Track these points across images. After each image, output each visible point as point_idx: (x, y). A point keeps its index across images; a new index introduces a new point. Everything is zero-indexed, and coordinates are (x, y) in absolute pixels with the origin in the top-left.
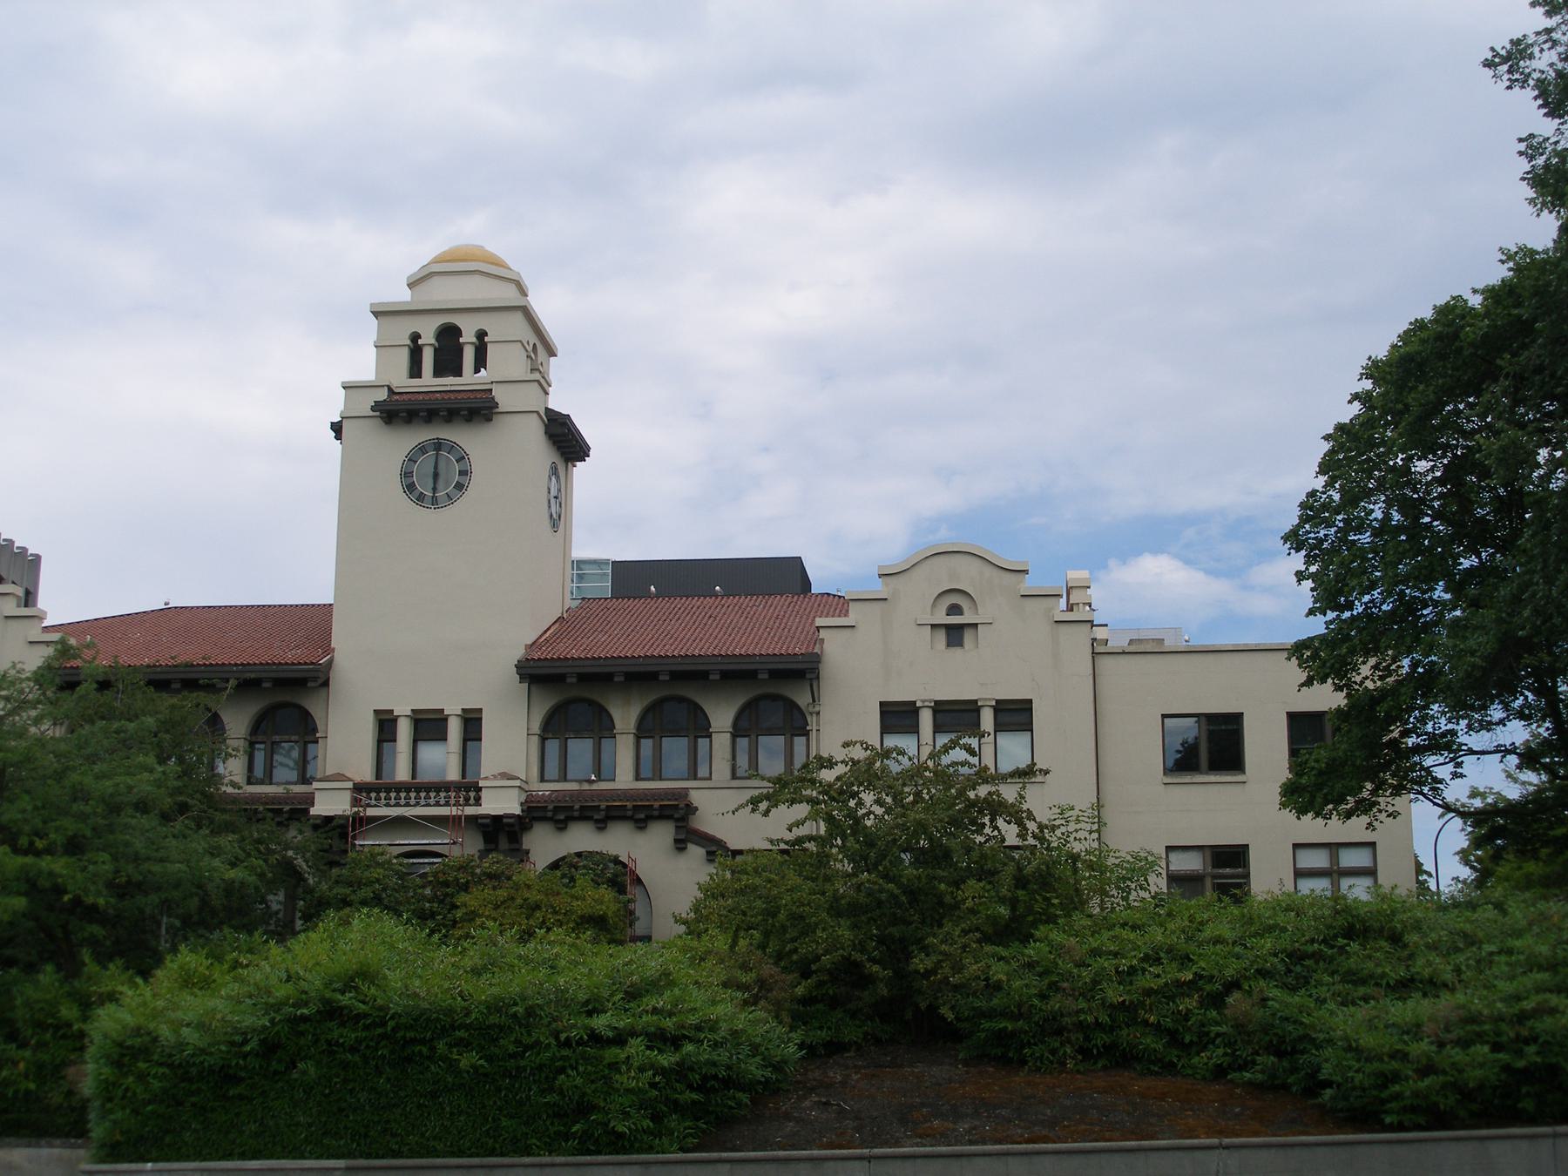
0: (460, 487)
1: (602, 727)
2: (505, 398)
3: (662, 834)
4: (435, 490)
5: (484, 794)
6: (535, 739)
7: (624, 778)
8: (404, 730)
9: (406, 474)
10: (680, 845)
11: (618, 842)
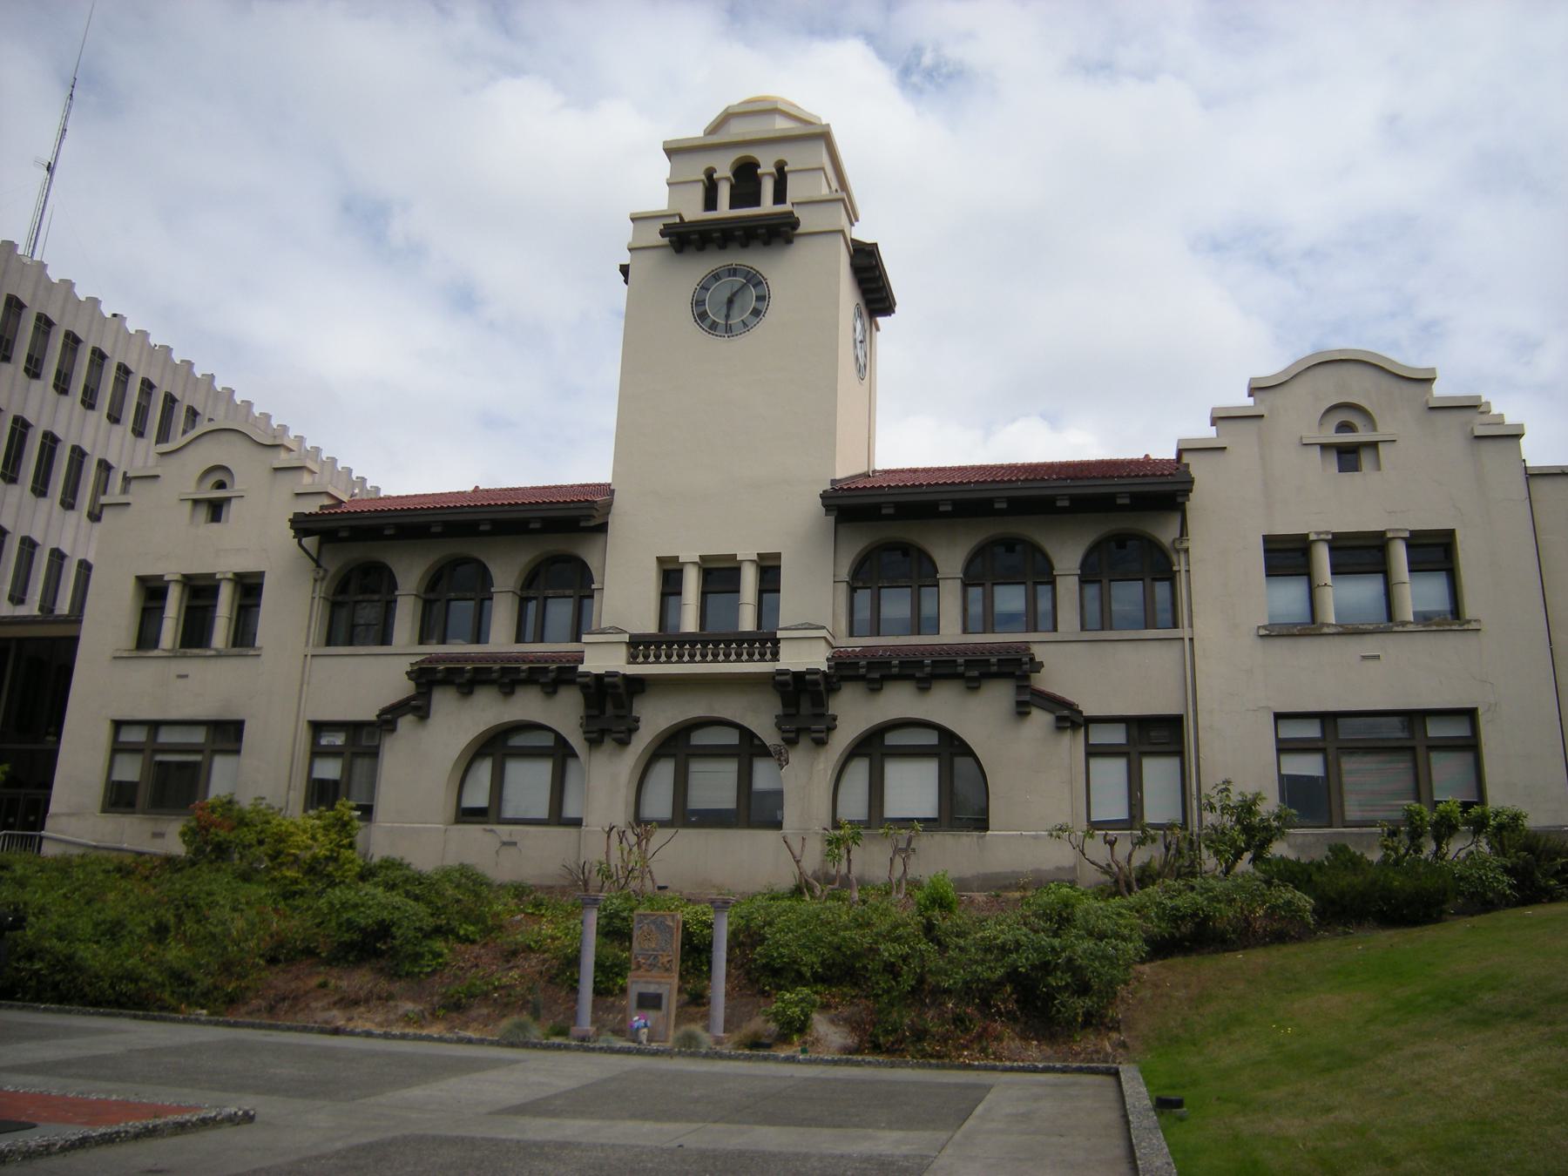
0: (756, 313)
1: (923, 574)
2: (809, 220)
3: (999, 696)
4: (727, 317)
5: (782, 645)
6: (843, 588)
7: (951, 632)
8: (692, 583)
9: (698, 303)
10: (1022, 710)
11: (944, 706)
